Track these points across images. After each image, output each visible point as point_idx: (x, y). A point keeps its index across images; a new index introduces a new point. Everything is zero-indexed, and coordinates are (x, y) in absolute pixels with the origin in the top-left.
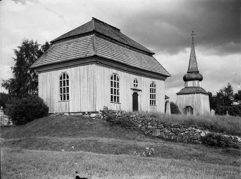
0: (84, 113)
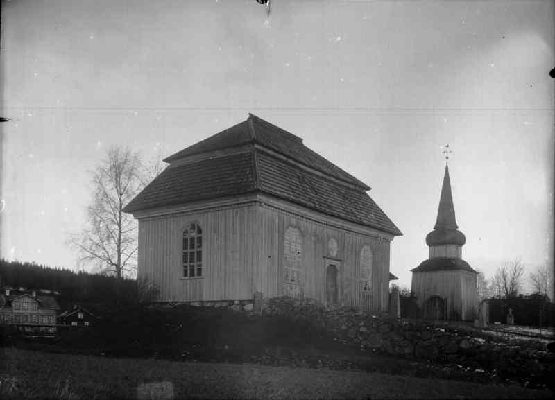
0: (233, 302)
